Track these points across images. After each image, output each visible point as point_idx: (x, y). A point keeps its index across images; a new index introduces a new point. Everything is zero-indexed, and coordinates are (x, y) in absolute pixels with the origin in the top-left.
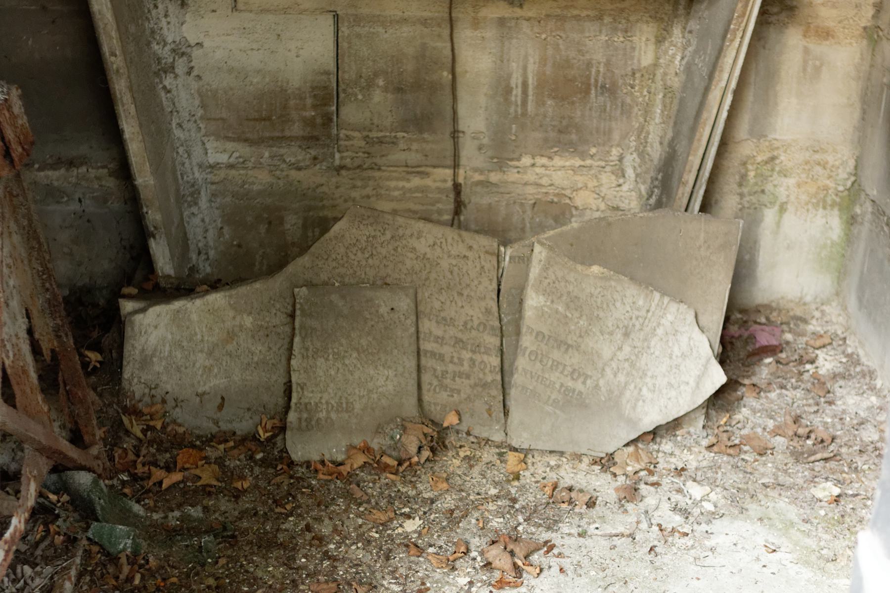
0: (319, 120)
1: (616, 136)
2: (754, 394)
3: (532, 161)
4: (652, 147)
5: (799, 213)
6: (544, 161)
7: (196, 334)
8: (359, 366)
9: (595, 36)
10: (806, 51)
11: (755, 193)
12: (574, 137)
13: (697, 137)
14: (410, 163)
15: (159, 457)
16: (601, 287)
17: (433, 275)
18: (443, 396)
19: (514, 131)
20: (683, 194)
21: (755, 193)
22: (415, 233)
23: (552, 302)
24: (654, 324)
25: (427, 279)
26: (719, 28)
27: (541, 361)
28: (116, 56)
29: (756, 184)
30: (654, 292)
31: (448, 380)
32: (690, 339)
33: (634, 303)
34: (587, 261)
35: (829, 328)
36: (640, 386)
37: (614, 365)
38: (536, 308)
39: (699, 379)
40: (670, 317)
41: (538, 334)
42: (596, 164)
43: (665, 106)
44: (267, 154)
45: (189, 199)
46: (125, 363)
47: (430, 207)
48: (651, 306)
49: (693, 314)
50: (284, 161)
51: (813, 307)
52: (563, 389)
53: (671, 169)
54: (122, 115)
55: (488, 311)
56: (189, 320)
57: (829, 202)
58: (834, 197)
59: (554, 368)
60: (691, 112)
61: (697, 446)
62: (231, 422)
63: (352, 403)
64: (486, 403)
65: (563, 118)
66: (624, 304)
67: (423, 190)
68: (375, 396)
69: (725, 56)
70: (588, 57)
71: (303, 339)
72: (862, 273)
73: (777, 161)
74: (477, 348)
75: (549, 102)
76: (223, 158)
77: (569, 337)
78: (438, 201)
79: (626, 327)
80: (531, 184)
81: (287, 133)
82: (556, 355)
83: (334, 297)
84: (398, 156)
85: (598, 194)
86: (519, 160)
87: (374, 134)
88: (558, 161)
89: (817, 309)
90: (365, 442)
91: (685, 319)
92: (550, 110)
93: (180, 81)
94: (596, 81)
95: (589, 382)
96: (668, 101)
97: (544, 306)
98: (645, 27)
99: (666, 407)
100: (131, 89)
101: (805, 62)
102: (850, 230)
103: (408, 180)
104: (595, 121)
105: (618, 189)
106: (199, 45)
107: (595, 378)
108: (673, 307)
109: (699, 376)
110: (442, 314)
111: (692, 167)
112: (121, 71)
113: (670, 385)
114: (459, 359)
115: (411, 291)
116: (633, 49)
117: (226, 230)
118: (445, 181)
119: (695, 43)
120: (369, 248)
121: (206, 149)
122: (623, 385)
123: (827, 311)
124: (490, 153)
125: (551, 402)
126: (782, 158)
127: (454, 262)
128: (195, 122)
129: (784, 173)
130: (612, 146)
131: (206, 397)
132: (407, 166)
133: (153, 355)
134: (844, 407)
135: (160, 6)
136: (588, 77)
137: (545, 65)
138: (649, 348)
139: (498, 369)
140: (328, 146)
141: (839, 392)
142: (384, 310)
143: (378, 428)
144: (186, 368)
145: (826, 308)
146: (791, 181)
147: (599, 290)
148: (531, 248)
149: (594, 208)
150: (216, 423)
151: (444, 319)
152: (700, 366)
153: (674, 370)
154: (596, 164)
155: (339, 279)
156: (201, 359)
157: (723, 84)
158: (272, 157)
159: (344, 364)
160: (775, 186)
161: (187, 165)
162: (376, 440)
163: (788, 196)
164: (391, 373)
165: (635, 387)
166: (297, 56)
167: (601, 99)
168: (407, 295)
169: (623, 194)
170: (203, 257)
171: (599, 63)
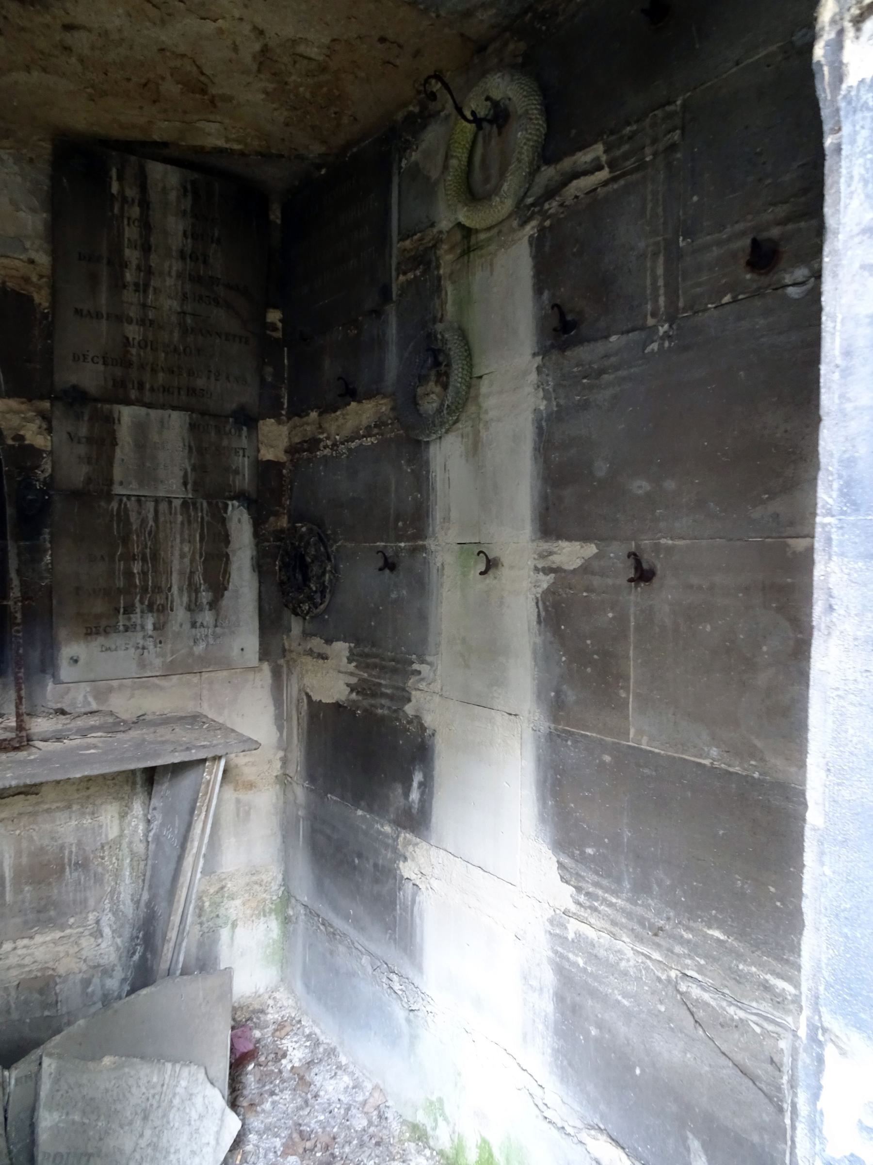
1: (91, 903)
2: (254, 1113)
3: (14, 946)
4: (124, 905)
5: (246, 925)
6: (26, 942)
9: (65, 823)
10: (238, 801)
16: (115, 1078)
20: (168, 950)
24: (170, 1096)
26: (185, 806)
29: (212, 912)
30: (166, 1063)
32: (204, 1097)
34: (96, 1057)
35: (283, 1013)
38: (51, 1127)
40: (183, 1083)
42: (76, 931)
43: (133, 869)
48: (165, 1078)
51: (266, 996)
53: (152, 928)
57: (267, 910)
58: (271, 905)
60: (166, 873)
65: (41, 899)
66: (140, 1087)
69: (194, 829)
70: (60, 842)
72: (304, 963)
73: (226, 889)
75: (27, 889)
79: (144, 1110)
80: (14, 967)
85: (80, 958)
88: (39, 939)
92: (28, 895)
94: (70, 860)
96: (135, 863)
97: (59, 1122)
98: (109, 807)
101: (238, 809)
102: (285, 928)
105: (97, 948)
108: (185, 1072)
109: (217, 1131)
113: (193, 1153)
116: (101, 827)
119: (161, 817)
123: (278, 997)
126: (229, 885)
129: (232, 897)
130: (89, 912)
134: (327, 1097)
136: (63, 858)
137: (21, 857)
141: (318, 1080)
145: (277, 995)
146: (238, 902)
147: (113, 1082)
148: (38, 1062)
149: (77, 970)
154: (76, 931)
157: (194, 851)
160: (227, 909)
167: (75, 874)
169: (103, 951)
171: (71, 845)
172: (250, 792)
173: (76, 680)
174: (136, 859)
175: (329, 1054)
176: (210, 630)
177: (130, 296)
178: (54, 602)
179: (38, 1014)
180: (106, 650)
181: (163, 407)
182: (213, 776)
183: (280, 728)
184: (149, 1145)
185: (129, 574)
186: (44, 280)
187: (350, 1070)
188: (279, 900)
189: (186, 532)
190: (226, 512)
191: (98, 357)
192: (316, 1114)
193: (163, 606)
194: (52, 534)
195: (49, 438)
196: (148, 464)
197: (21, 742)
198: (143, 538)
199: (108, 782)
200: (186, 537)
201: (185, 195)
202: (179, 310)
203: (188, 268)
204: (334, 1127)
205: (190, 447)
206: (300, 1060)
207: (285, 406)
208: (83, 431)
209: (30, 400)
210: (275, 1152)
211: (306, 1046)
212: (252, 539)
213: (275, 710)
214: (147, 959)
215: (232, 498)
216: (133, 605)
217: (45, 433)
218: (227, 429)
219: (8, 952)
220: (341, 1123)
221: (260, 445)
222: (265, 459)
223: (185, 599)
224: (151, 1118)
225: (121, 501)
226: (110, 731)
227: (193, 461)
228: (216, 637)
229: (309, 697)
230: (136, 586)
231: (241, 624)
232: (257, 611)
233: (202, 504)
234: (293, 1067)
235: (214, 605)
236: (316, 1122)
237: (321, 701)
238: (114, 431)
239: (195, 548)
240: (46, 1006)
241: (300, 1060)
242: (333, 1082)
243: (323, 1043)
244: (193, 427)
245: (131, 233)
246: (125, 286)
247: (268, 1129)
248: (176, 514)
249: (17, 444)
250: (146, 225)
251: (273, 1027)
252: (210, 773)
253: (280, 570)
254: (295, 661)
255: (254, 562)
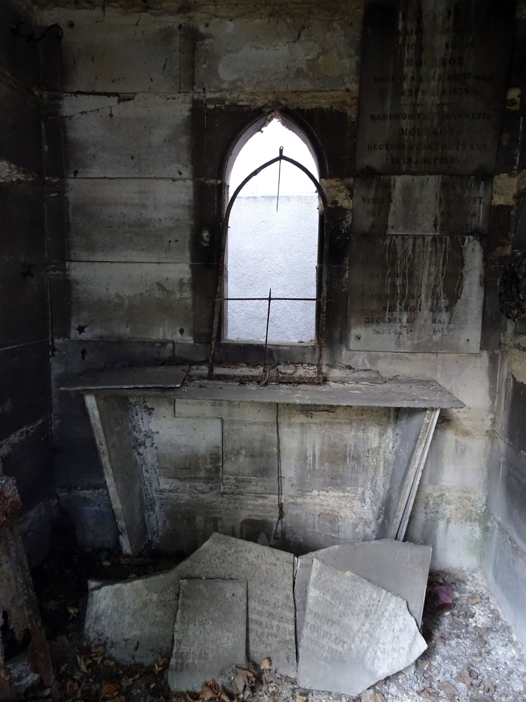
0: (213, 470)
1: (360, 481)
4: (379, 487)
6: (324, 493)
7: (126, 604)
8: (213, 630)
10: (457, 442)
11: (433, 512)
12: (339, 481)
13: (403, 493)
14: (257, 492)
15: (93, 687)
17: (257, 574)
18: (262, 647)
19: (309, 477)
20: (396, 522)
21: (433, 512)
22: (248, 550)
23: (324, 594)
25: (254, 576)
26: (413, 436)
27: (317, 632)
28: (102, 445)
29: (434, 508)
31: (265, 638)
32: (404, 619)
33: (371, 596)
34: (343, 569)
35: (478, 588)
36: (376, 649)
37: (360, 635)
39: (411, 645)
40: (392, 606)
41: (315, 614)
44: (188, 486)
45: (149, 507)
46: (86, 619)
47: (267, 514)
49: (406, 604)
50: (196, 489)
51: (468, 573)
52: (330, 650)
54: (106, 474)
55: (287, 597)
56: (123, 595)
57: (473, 518)
59: (325, 636)
61: (412, 690)
62: (142, 657)
63: (207, 654)
64: (286, 653)
67: (264, 506)
68: (221, 650)
69: (417, 452)
71: (182, 612)
72: (495, 562)
73: (445, 497)
74: (281, 619)
76: (167, 487)
77: (334, 616)
78: (271, 511)
79: (367, 611)
81: (198, 476)
82: (326, 628)
83: (202, 586)
84: (251, 488)
86: (311, 492)
87: (240, 477)
88: (331, 493)
89: (470, 575)
90: (214, 680)
91: (401, 607)
93: (147, 449)
95: (345, 646)
96: (386, 465)
98: (373, 428)
99: (392, 664)
100: (110, 461)
101: (457, 447)
103: (256, 501)
104: (349, 474)
106: (157, 432)
107: (349, 643)
108: (394, 599)
110: (262, 598)
111: (401, 508)
112: (105, 452)
113: (394, 649)
114: (271, 625)
115: (244, 584)
116: (368, 439)
117: (167, 522)
118: (275, 501)
120: (222, 557)
121: (159, 482)
122: (366, 648)
124: (297, 488)
125: (323, 658)
126: (447, 495)
127: (269, 567)
128: (154, 469)
129: (449, 503)
131: (129, 641)
132: (256, 493)
133: (102, 615)
135: (139, 414)
136: (346, 452)
138: (380, 624)
139: (293, 632)
140: (218, 482)
141: (493, 643)
142: (228, 595)
143: (221, 672)
144: (119, 623)
146: (452, 507)
149: (350, 518)
150: (133, 658)
151: (263, 600)
152: (411, 637)
153: (396, 640)
155: (205, 574)
156: (128, 619)
157: (416, 466)
158: (190, 487)
159: (204, 628)
160: (444, 509)
161: (149, 490)
162: (220, 679)
163: (451, 515)
164: (231, 635)
165: (373, 650)
166: (204, 439)
167: (352, 463)
168: (242, 586)
169: (365, 511)
170: (156, 535)
171: (351, 445)
172: (466, 438)
173: (359, 349)
174: (387, 462)
175: (504, 629)
176: (445, 326)
177: (405, 100)
178: (349, 302)
179: (329, 534)
180: (377, 333)
181: (423, 173)
182: (431, 421)
183: (493, 398)
184: (367, 632)
185: (393, 286)
186: (354, 100)
187: (518, 647)
188: (482, 514)
189: (434, 259)
190: (463, 244)
191: (383, 145)
192: (486, 664)
193: (414, 307)
194: (349, 260)
195: (351, 201)
196: (411, 213)
197: (319, 380)
198: (404, 263)
199: (374, 413)
200: (433, 262)
201: (449, 17)
202: (439, 102)
203: (447, 70)
204: (497, 679)
205: (440, 200)
206: (483, 624)
207: (517, 163)
208: (371, 195)
209: (342, 179)
210: (451, 675)
211: (489, 617)
212: (481, 263)
213: (490, 385)
214: (385, 524)
215: (468, 234)
216: (395, 306)
217: (349, 198)
218: (469, 184)
219: (315, 496)
220: (503, 680)
221: (494, 194)
222: (497, 204)
223: (429, 304)
224: (370, 617)
225: (392, 238)
226: (372, 381)
227: (442, 210)
228: (449, 330)
229: (514, 379)
230: (398, 294)
231: (468, 323)
232: (481, 314)
233: (446, 239)
234: (476, 627)
235: (449, 308)
236: (484, 670)
237: (522, 382)
238: (390, 193)
239: (439, 270)
240: (333, 531)
241: (483, 624)
242: (503, 648)
243: (502, 620)
244: (444, 185)
245: (409, 55)
246: (402, 94)
247: (450, 658)
248: (427, 246)
249: (333, 206)
250: (420, 47)
251: (469, 595)
252: (429, 418)
253: (500, 285)
254: (507, 352)
255: (482, 280)
